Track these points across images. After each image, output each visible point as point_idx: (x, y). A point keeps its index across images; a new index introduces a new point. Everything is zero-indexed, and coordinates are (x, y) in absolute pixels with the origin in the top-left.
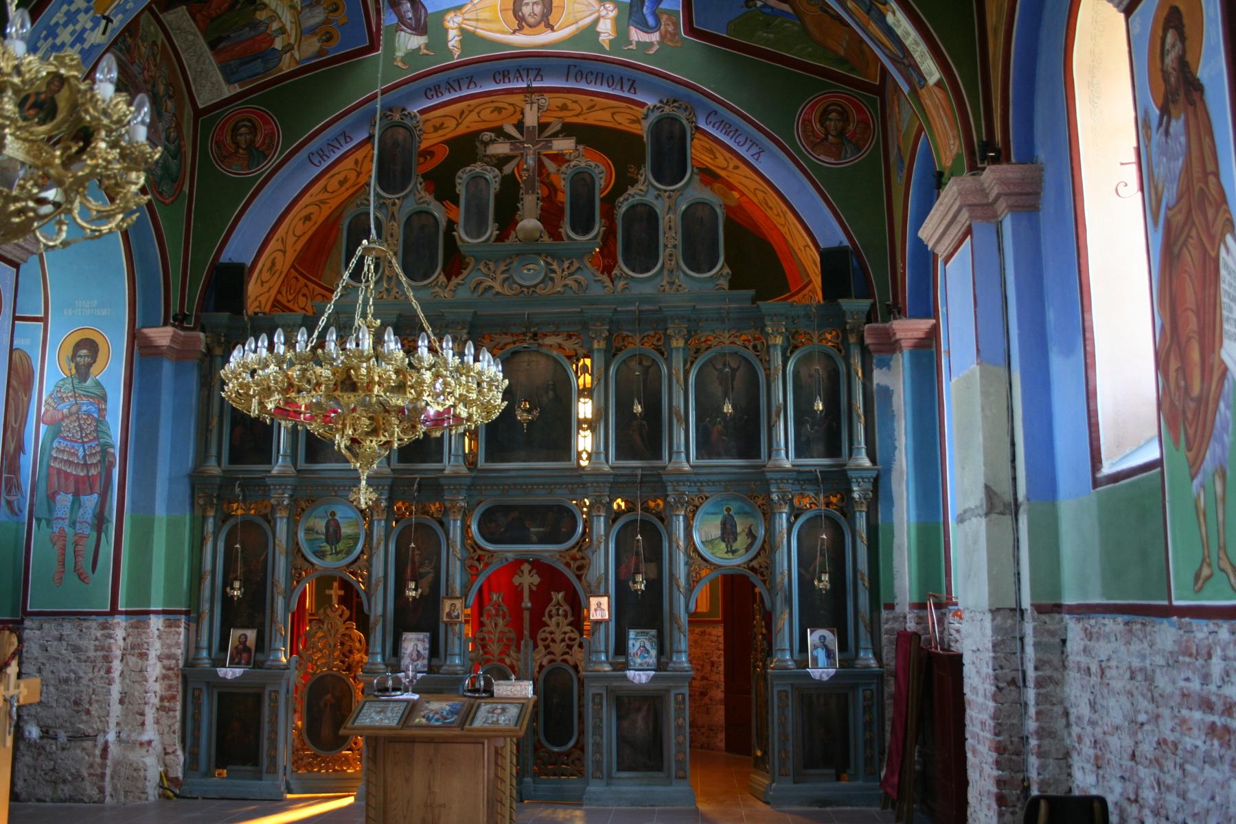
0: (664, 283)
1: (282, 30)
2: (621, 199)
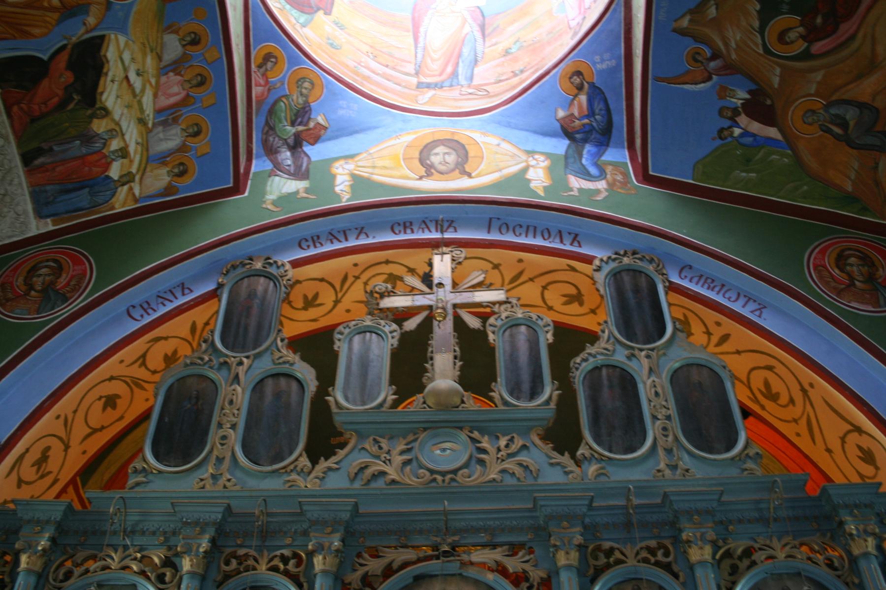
0: (662, 466)
1: (123, 153)
2: (578, 360)
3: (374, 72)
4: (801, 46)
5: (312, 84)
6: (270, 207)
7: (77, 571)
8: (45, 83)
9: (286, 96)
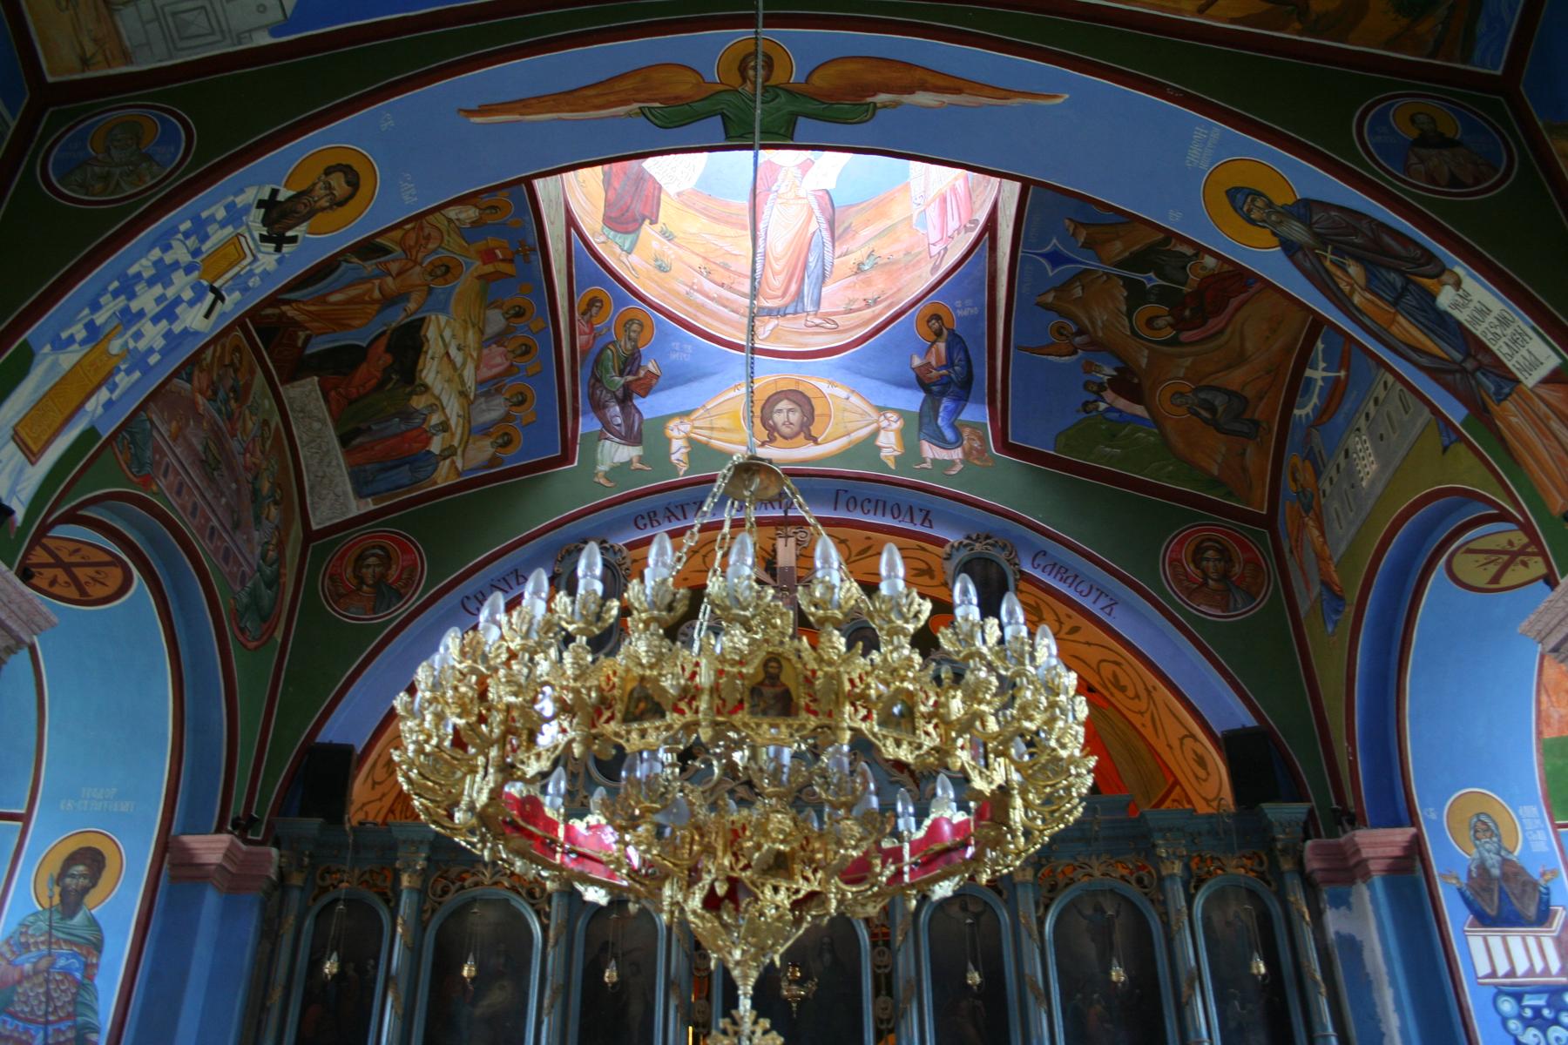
1: (444, 427)
3: (708, 297)
4: (1169, 333)
5: (641, 325)
6: (602, 481)
7: (453, 888)
8: (364, 367)
9: (613, 343)
